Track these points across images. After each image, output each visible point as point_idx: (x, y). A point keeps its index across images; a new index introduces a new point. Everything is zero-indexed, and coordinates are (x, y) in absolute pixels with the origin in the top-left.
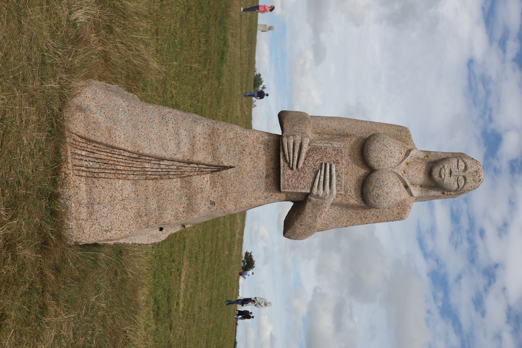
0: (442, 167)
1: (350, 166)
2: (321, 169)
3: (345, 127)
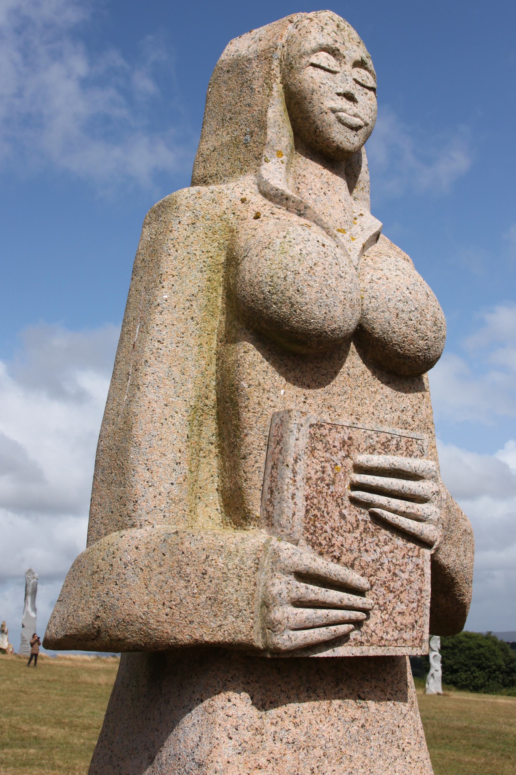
0: (332, 117)
1: (335, 401)
2: (367, 505)
3: (180, 401)
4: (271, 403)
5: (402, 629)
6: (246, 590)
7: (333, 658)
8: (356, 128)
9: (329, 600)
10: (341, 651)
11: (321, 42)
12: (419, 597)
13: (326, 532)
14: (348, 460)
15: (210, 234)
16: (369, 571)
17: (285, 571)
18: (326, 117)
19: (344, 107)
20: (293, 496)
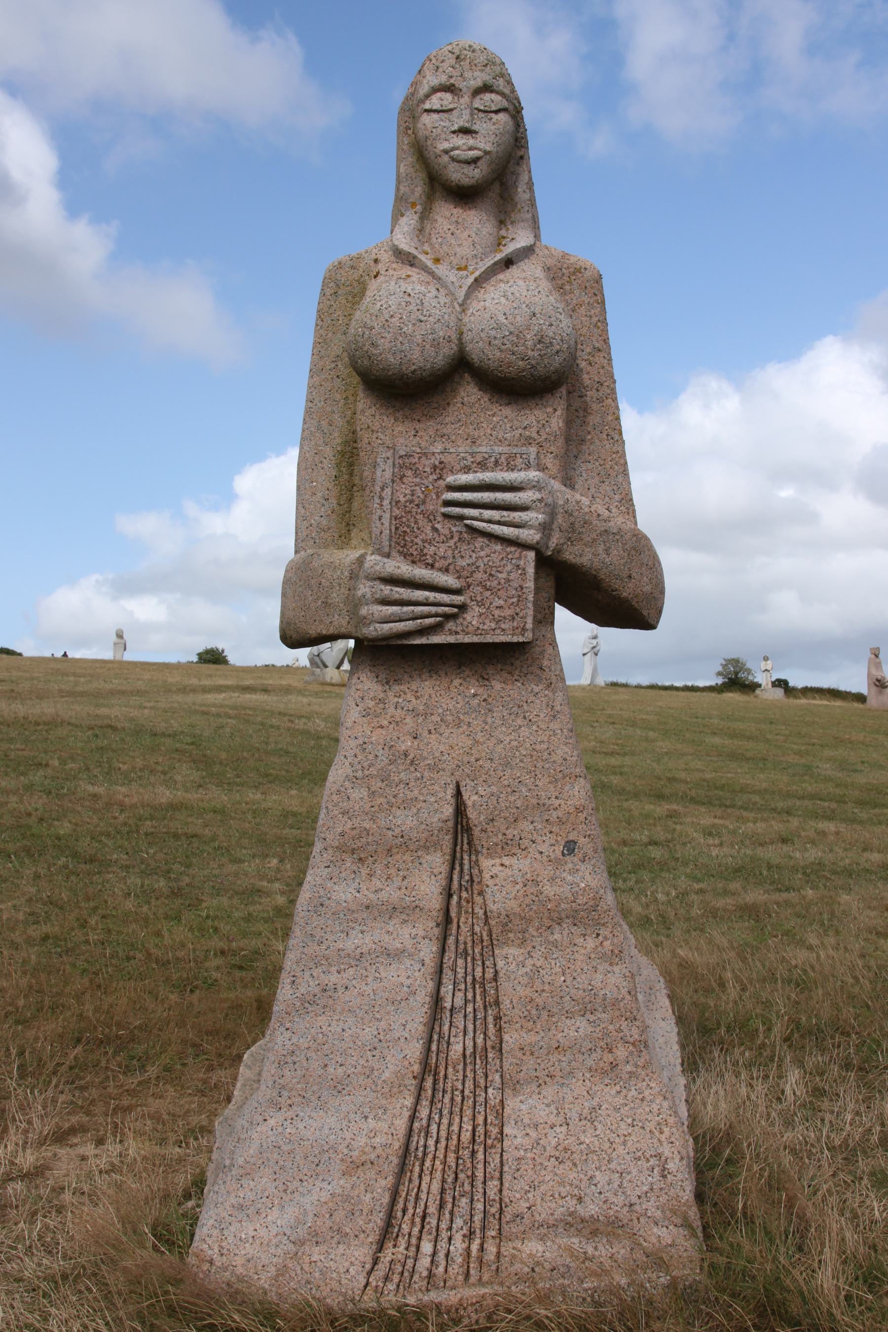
0: (446, 158)
2: (461, 518)
4: (380, 442)
5: (500, 621)
6: (343, 594)
7: (427, 645)
8: (475, 161)
9: (414, 599)
10: (436, 639)
11: (432, 84)
12: (520, 593)
13: (417, 544)
14: (441, 482)
15: (350, 299)
16: (465, 573)
17: (368, 578)
18: (440, 160)
19: (457, 145)
20: (380, 518)
